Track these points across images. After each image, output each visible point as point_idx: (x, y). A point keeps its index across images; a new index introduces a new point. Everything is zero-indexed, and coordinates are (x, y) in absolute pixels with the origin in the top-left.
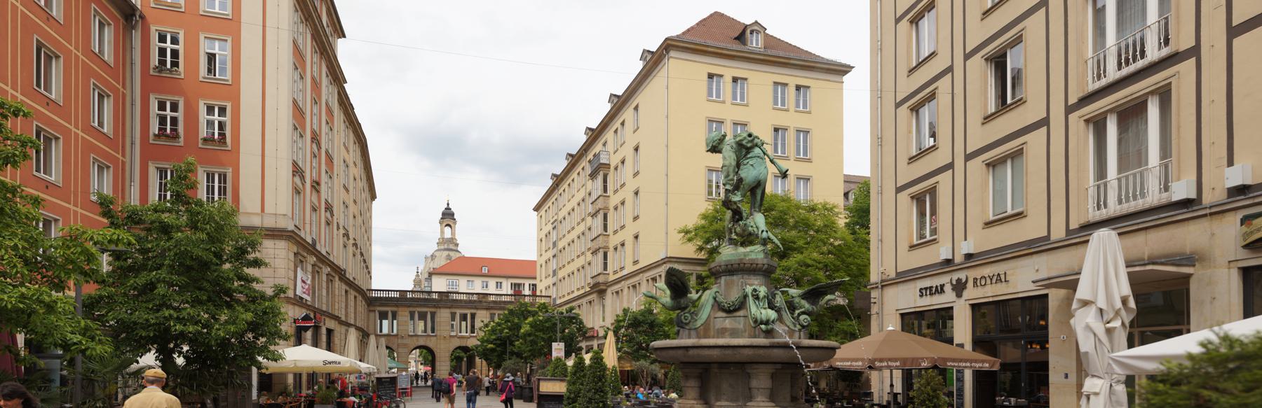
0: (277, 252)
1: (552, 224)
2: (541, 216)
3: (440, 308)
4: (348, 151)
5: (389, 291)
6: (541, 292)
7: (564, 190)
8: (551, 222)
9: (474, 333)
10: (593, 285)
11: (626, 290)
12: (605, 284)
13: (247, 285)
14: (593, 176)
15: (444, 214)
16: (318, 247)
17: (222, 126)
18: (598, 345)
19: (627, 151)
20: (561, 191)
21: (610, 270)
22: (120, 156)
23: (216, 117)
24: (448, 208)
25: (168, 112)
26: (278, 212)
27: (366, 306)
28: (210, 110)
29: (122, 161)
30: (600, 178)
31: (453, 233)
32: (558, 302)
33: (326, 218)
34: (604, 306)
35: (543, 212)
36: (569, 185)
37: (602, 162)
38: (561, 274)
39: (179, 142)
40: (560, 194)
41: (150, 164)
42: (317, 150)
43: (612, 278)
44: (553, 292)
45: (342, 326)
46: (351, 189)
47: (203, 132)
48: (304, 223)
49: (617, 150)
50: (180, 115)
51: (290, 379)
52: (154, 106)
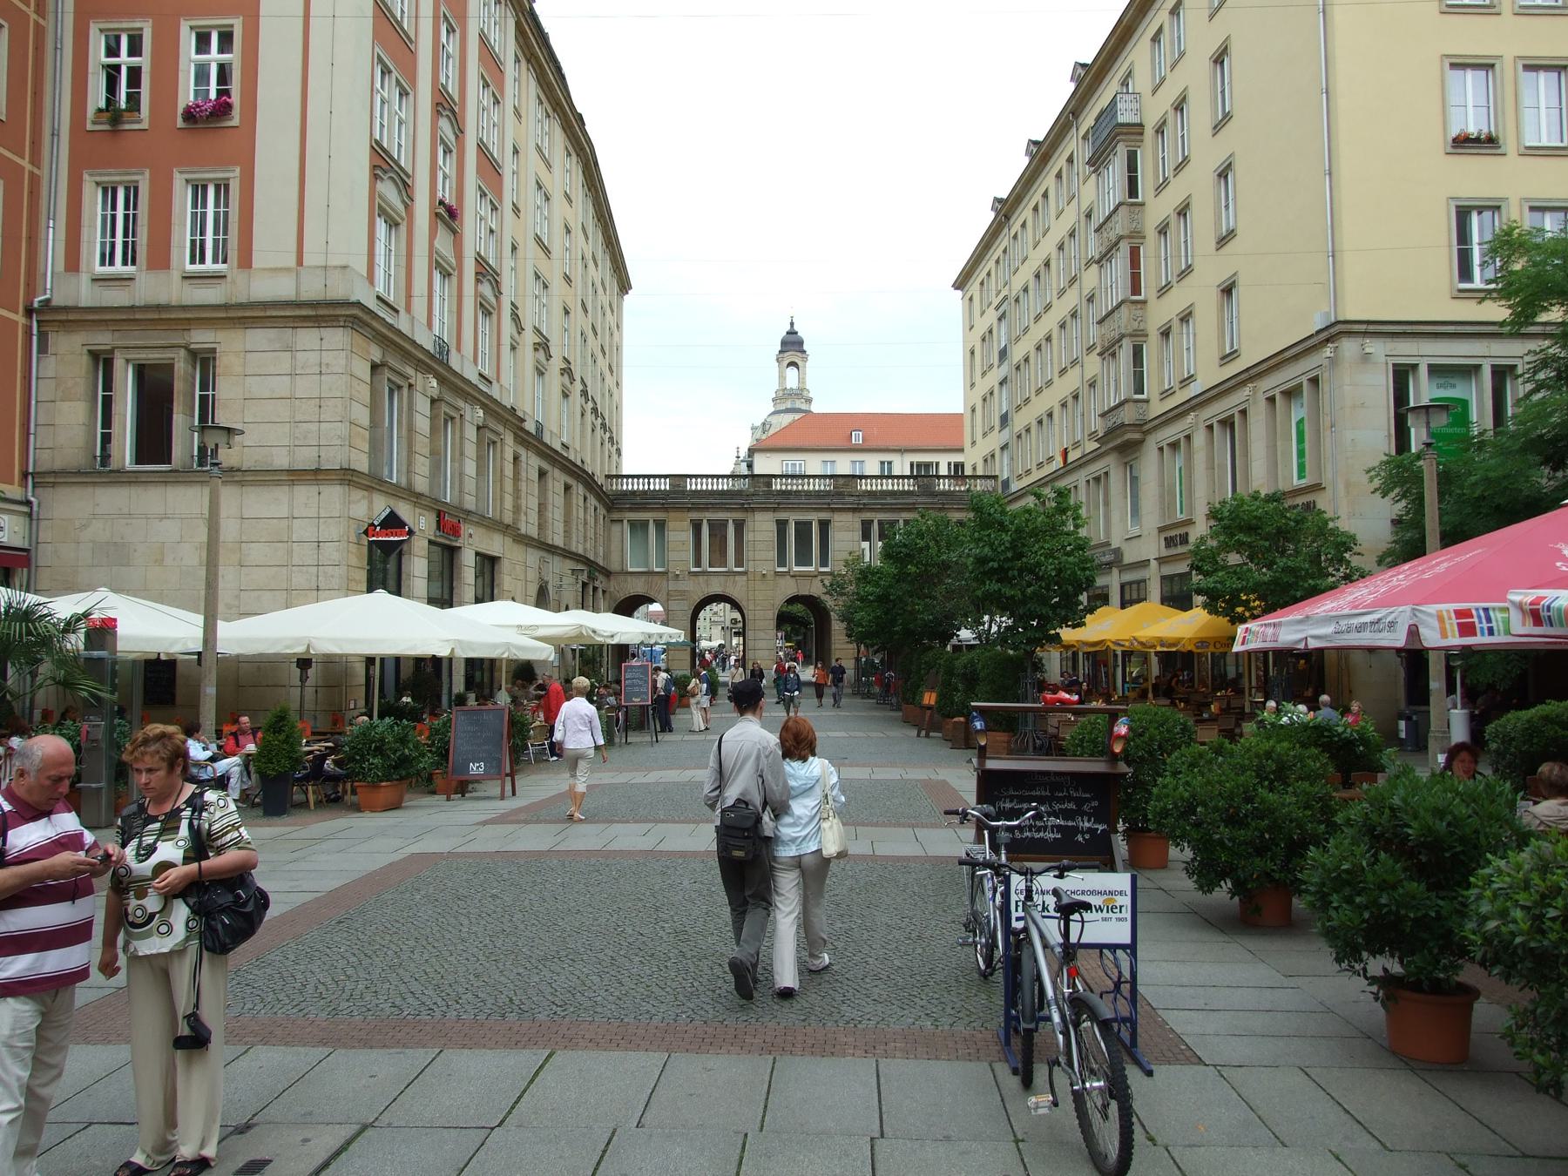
0: (328, 357)
1: (997, 308)
2: (971, 299)
3: (753, 510)
4: (549, 166)
5: (649, 477)
6: (974, 469)
7: (1024, 225)
8: (994, 306)
9: (826, 566)
10: (1106, 434)
11: (1199, 439)
12: (1137, 426)
13: (1494, 746)
14: (1098, 162)
15: (784, 343)
16: (455, 362)
17: (224, 73)
18: (1122, 587)
19: (1195, 74)
20: (1016, 227)
21: (1151, 388)
22: (25, 163)
23: (214, 56)
24: (792, 333)
25: (124, 59)
26: (329, 264)
27: (602, 511)
28: (203, 42)
29: (32, 174)
30: (1116, 170)
31: (801, 380)
32: (1015, 486)
33: (477, 294)
34: (1135, 480)
35: (974, 287)
36: (1036, 209)
37: (1121, 119)
38: (1019, 422)
39: (139, 122)
40: (1015, 237)
41: (86, 177)
42: (452, 138)
43: (1157, 408)
44: (1003, 469)
45: (530, 550)
46: (556, 250)
47: (187, 94)
48: (409, 297)
49: (1163, 80)
50: (144, 61)
51: (360, 669)
52: (98, 54)
